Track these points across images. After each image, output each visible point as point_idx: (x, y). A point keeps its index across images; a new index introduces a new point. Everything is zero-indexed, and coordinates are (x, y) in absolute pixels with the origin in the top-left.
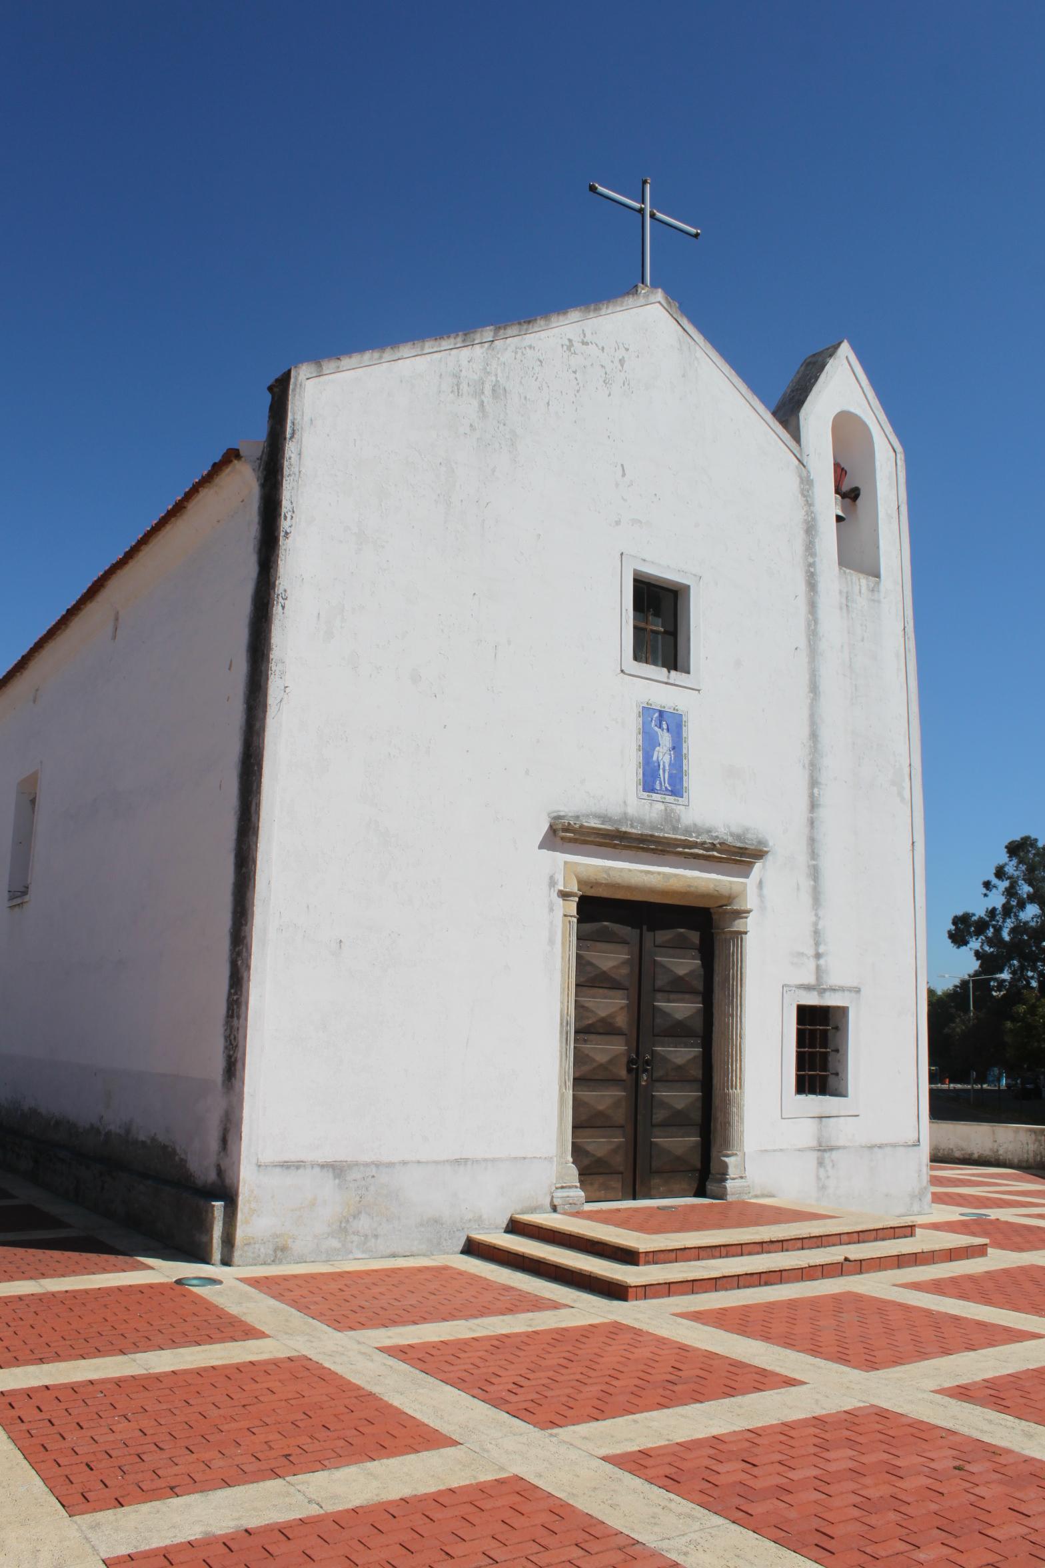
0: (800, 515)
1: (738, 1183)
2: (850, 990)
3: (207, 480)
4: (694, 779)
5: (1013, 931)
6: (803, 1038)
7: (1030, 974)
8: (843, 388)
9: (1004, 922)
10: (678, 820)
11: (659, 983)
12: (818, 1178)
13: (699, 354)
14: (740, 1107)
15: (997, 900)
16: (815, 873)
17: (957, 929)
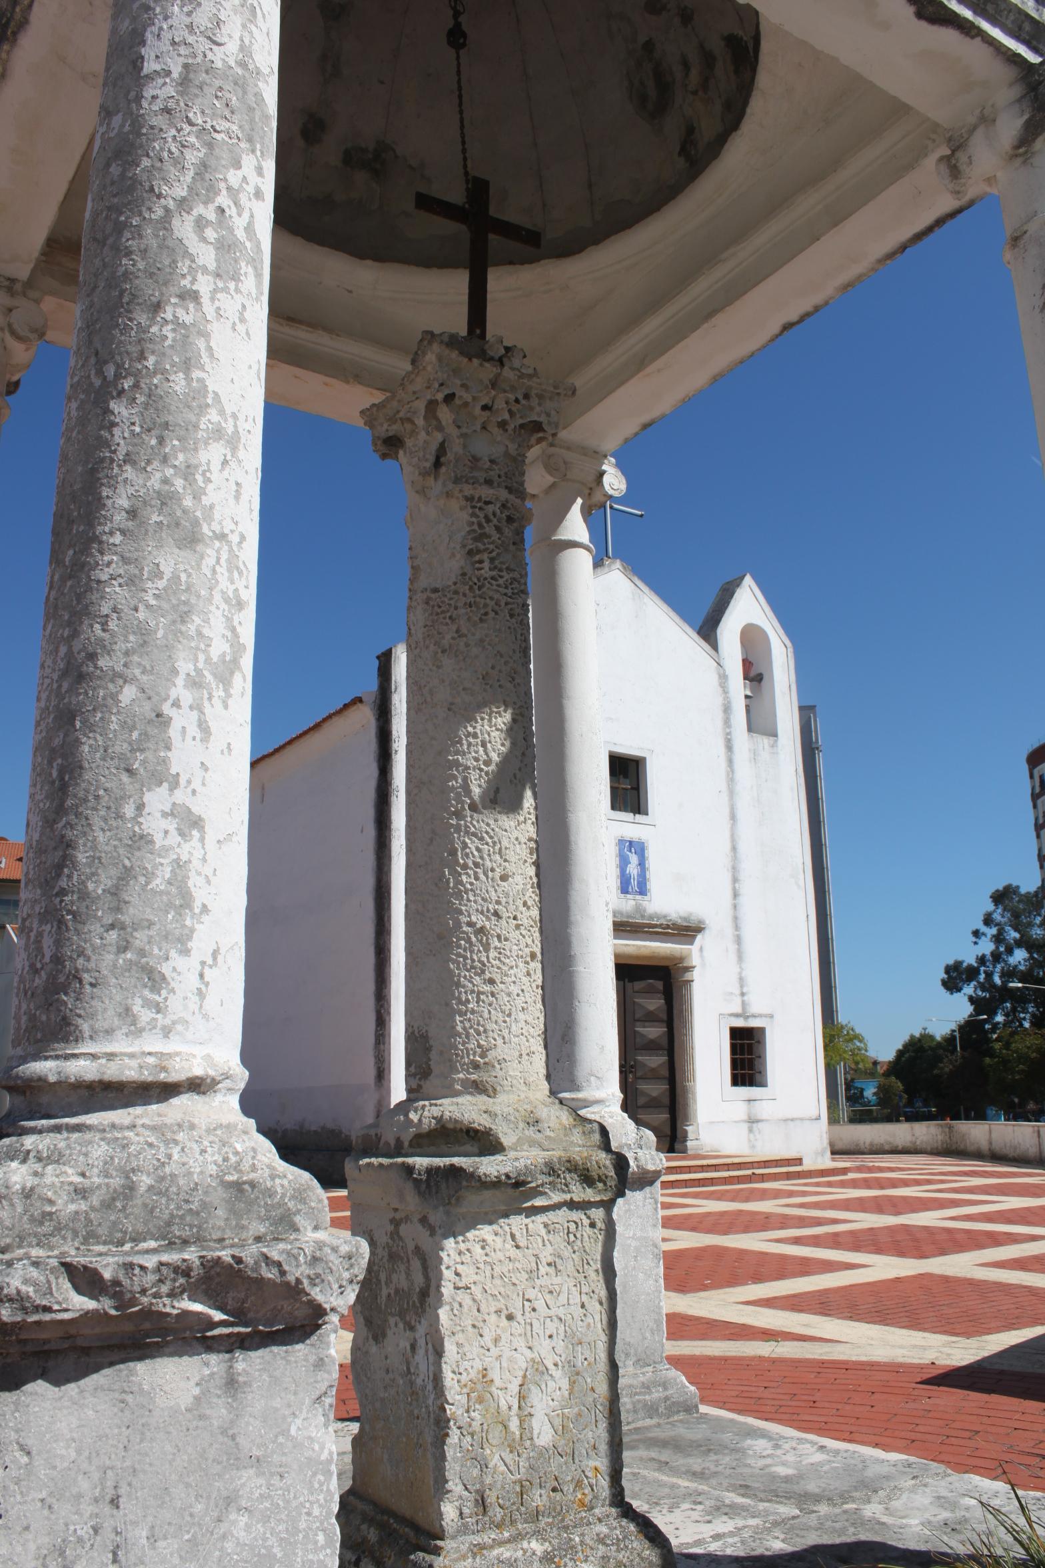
0: (719, 701)
1: (694, 1143)
2: (766, 1016)
3: (339, 712)
4: (653, 884)
5: (1001, 977)
7: (1022, 1015)
8: (748, 607)
9: (994, 967)
11: (637, 1016)
12: (749, 1141)
13: (646, 600)
14: (694, 1094)
15: (986, 947)
16: (738, 940)
17: (950, 977)
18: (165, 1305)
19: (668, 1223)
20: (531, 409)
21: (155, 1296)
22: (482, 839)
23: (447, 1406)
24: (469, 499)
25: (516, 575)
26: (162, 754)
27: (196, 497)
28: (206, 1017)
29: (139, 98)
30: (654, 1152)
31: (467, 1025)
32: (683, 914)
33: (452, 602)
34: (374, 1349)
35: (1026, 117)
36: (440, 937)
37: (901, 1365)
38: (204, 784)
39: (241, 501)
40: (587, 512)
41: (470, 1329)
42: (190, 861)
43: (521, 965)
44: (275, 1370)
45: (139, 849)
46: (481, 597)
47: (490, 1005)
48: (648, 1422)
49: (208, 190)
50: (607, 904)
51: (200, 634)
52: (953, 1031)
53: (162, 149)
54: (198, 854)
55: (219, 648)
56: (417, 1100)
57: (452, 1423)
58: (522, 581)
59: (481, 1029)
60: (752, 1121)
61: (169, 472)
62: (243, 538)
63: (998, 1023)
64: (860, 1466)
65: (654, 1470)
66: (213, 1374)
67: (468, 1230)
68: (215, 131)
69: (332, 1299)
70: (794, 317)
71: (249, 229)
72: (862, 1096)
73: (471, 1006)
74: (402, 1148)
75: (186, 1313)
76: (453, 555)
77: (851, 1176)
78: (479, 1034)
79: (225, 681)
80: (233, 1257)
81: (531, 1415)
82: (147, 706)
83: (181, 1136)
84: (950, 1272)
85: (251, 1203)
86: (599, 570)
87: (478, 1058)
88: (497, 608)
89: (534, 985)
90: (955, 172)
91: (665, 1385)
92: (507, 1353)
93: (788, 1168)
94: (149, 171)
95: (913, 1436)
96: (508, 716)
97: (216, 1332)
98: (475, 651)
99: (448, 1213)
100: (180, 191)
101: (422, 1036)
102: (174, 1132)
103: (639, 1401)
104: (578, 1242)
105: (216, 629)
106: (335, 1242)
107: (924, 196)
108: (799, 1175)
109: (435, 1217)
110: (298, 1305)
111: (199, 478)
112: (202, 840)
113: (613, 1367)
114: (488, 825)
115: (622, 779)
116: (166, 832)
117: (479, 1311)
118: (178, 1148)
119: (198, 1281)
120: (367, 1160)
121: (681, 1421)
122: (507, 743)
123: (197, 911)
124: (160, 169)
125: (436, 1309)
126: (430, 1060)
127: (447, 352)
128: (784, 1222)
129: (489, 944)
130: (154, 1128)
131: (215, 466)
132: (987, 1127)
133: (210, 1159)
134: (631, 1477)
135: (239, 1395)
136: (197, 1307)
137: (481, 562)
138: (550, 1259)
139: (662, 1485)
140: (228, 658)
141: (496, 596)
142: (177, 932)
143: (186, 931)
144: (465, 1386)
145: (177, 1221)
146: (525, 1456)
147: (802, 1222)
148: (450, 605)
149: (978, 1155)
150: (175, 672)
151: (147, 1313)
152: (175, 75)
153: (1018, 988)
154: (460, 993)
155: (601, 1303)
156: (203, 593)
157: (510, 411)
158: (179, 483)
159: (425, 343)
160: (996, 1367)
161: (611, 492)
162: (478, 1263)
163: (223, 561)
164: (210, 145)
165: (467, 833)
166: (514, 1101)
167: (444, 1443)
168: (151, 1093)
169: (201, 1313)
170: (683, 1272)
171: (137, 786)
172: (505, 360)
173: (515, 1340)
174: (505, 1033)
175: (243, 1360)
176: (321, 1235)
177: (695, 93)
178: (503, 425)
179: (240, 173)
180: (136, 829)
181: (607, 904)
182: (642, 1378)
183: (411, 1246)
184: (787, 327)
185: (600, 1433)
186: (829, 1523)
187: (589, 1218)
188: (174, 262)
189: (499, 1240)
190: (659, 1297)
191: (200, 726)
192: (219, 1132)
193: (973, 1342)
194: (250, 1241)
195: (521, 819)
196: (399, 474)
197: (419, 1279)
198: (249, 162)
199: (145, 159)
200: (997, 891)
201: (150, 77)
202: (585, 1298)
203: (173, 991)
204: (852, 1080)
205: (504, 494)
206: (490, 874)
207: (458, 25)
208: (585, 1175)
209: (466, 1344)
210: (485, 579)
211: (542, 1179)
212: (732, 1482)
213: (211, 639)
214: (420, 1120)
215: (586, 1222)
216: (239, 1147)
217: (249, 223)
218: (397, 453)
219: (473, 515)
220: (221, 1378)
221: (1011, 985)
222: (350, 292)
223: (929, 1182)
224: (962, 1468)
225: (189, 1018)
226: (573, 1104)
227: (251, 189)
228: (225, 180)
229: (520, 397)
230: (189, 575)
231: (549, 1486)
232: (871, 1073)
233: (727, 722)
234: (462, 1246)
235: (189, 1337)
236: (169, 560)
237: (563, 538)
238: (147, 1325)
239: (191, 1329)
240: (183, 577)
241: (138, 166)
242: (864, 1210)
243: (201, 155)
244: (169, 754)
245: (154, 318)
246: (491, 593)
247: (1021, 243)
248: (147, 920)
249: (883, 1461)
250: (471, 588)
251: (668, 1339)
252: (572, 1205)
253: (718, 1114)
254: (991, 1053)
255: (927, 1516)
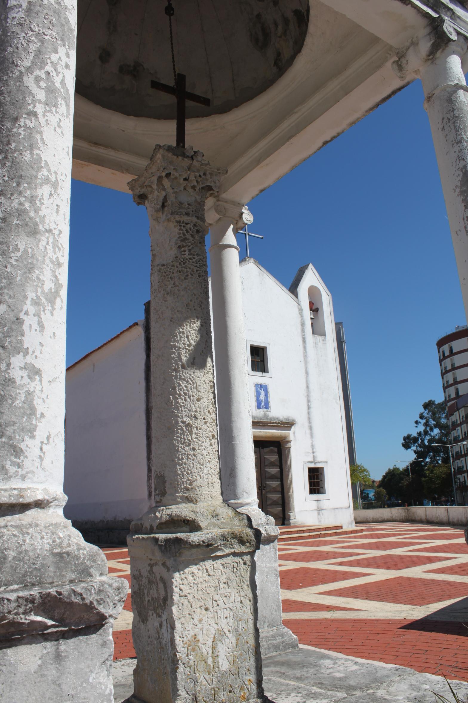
0: (299, 321)
1: (294, 520)
2: (324, 462)
3: (128, 330)
4: (272, 404)
5: (428, 442)
6: (310, 477)
8: (311, 278)
9: (425, 437)
10: (268, 416)
11: (266, 464)
13: (265, 276)
14: (293, 498)
15: (421, 428)
16: (311, 428)
18: (21, 619)
19: (281, 558)
20: (207, 180)
21: (16, 614)
22: (187, 382)
23: (177, 654)
24: (179, 222)
25: (201, 257)
26: (20, 338)
27: (36, 211)
28: (44, 469)
29: (6, 18)
30: (274, 527)
31: (183, 470)
32: (285, 417)
33: (171, 270)
34: (142, 626)
35: (432, 42)
36: (169, 429)
37: (390, 620)
38: (41, 353)
39: (59, 214)
40: (235, 231)
41: (187, 615)
42: (35, 392)
43: (208, 441)
44: (81, 648)
45: (8, 386)
46: (185, 268)
47: (193, 460)
48: (275, 653)
49: (41, 63)
50: (249, 412)
51: (38, 279)
52: (408, 466)
53: (18, 43)
54: (39, 388)
55: (48, 285)
56: (160, 506)
57: (180, 662)
58: (204, 260)
59: (189, 472)
60: (319, 510)
61: (22, 199)
62: (60, 232)
63: (427, 462)
64: (374, 671)
65: (278, 677)
66: (48, 653)
67: (185, 568)
68: (45, 34)
69: (109, 611)
70: (328, 139)
71: (63, 83)
72: (368, 497)
73: (184, 461)
74: (153, 529)
75: (33, 622)
76: (171, 249)
77: (364, 533)
78: (188, 474)
79: (52, 302)
80: (57, 592)
81: (218, 656)
82: (12, 315)
83: (31, 530)
84: (410, 576)
85: (67, 563)
86: (243, 263)
87: (188, 486)
88: (192, 273)
89: (214, 450)
90: (400, 68)
91: (282, 636)
92: (206, 627)
93: (336, 530)
94: (11, 53)
95: (397, 654)
96: (198, 324)
97: (49, 631)
98: (182, 293)
99: (175, 560)
100: (27, 63)
101: (161, 476)
102: (27, 528)
103: (270, 644)
104: (238, 572)
105: (47, 276)
106: (111, 582)
107: (387, 80)
108: (341, 533)
109: (170, 563)
110: (92, 615)
111: (38, 202)
112: (41, 381)
113: (257, 630)
114: (190, 375)
115: (256, 357)
116: (22, 377)
117: (191, 607)
118: (29, 537)
119: (38, 605)
120: (137, 536)
121: (290, 652)
122: (199, 336)
123: (38, 416)
124: (17, 53)
125: (171, 607)
126: (165, 487)
127: (166, 153)
128: (335, 555)
129: (192, 431)
130: (17, 527)
131: (46, 196)
132: (424, 509)
133: (45, 542)
134: (267, 681)
135: (62, 663)
136: (39, 619)
137: (184, 251)
138: (225, 581)
139: (282, 684)
140: (53, 291)
141: (192, 267)
142: (28, 427)
143: (33, 427)
144: (186, 643)
145: (29, 574)
146: (215, 676)
147: (343, 555)
148: (170, 272)
149: (421, 522)
150: (26, 297)
151: (12, 623)
152: (24, 7)
153: (436, 446)
154: (179, 455)
155: (250, 601)
156: (40, 258)
157: (197, 181)
158: (27, 205)
159: (157, 150)
160: (434, 619)
161: (246, 222)
162: (190, 584)
163: (50, 243)
164: (42, 41)
165: (180, 379)
166: (205, 505)
167: (176, 672)
168: (16, 509)
169: (41, 622)
170: (289, 580)
171: (7, 354)
172: (194, 157)
173: (209, 620)
174: (201, 473)
175: (64, 644)
176: (103, 578)
177: (280, 37)
178: (193, 187)
179: (57, 56)
180: (7, 376)
181: (249, 412)
182: (271, 633)
183: (158, 577)
184: (325, 143)
185: (251, 663)
186: (361, 700)
187: (243, 560)
188: (25, 97)
189: (200, 572)
190: (278, 594)
191: (39, 324)
192: (51, 528)
193: (423, 608)
194: (67, 583)
195: (206, 372)
196: (147, 211)
197: (162, 593)
198: (62, 51)
199: (9, 47)
200: (425, 403)
201: (11, 8)
202: (242, 598)
203: (26, 457)
204: (363, 490)
205: (194, 219)
206: (192, 398)
207: (170, 5)
208: (241, 540)
209: (186, 623)
210: (187, 259)
211: (220, 542)
212: (315, 681)
213: (44, 281)
214: (161, 516)
215: (242, 562)
216: (61, 535)
217: (62, 80)
218: (144, 202)
219: (180, 229)
220: (53, 654)
221: (433, 445)
222: (123, 131)
223: (399, 535)
224: (422, 670)
225: (35, 470)
226: (234, 506)
227: (63, 63)
228: (50, 58)
229: (202, 175)
230: (33, 250)
231: (228, 690)
232: (372, 487)
233: (303, 330)
234: (183, 576)
235: (34, 634)
236: (22, 242)
237: (225, 243)
238: (12, 629)
239: (36, 630)
240: (30, 251)
241: (6, 51)
242: (371, 549)
243: (38, 46)
244: (23, 338)
245: (15, 124)
246: (190, 266)
247: (432, 99)
248: (13, 421)
249: (385, 668)
250: (180, 264)
251: (283, 612)
252: (235, 554)
253: (304, 507)
254: (425, 476)
255: (407, 694)
